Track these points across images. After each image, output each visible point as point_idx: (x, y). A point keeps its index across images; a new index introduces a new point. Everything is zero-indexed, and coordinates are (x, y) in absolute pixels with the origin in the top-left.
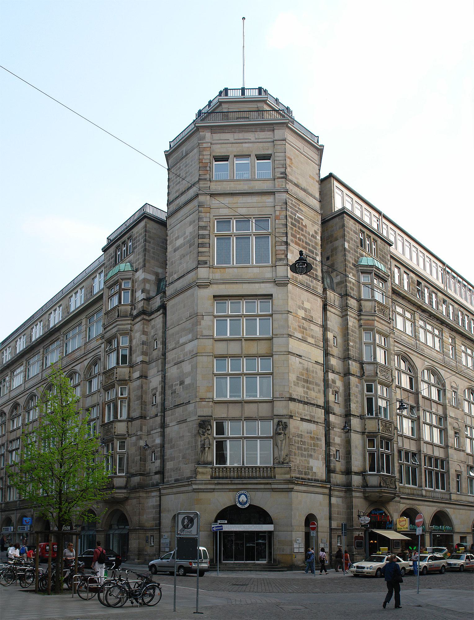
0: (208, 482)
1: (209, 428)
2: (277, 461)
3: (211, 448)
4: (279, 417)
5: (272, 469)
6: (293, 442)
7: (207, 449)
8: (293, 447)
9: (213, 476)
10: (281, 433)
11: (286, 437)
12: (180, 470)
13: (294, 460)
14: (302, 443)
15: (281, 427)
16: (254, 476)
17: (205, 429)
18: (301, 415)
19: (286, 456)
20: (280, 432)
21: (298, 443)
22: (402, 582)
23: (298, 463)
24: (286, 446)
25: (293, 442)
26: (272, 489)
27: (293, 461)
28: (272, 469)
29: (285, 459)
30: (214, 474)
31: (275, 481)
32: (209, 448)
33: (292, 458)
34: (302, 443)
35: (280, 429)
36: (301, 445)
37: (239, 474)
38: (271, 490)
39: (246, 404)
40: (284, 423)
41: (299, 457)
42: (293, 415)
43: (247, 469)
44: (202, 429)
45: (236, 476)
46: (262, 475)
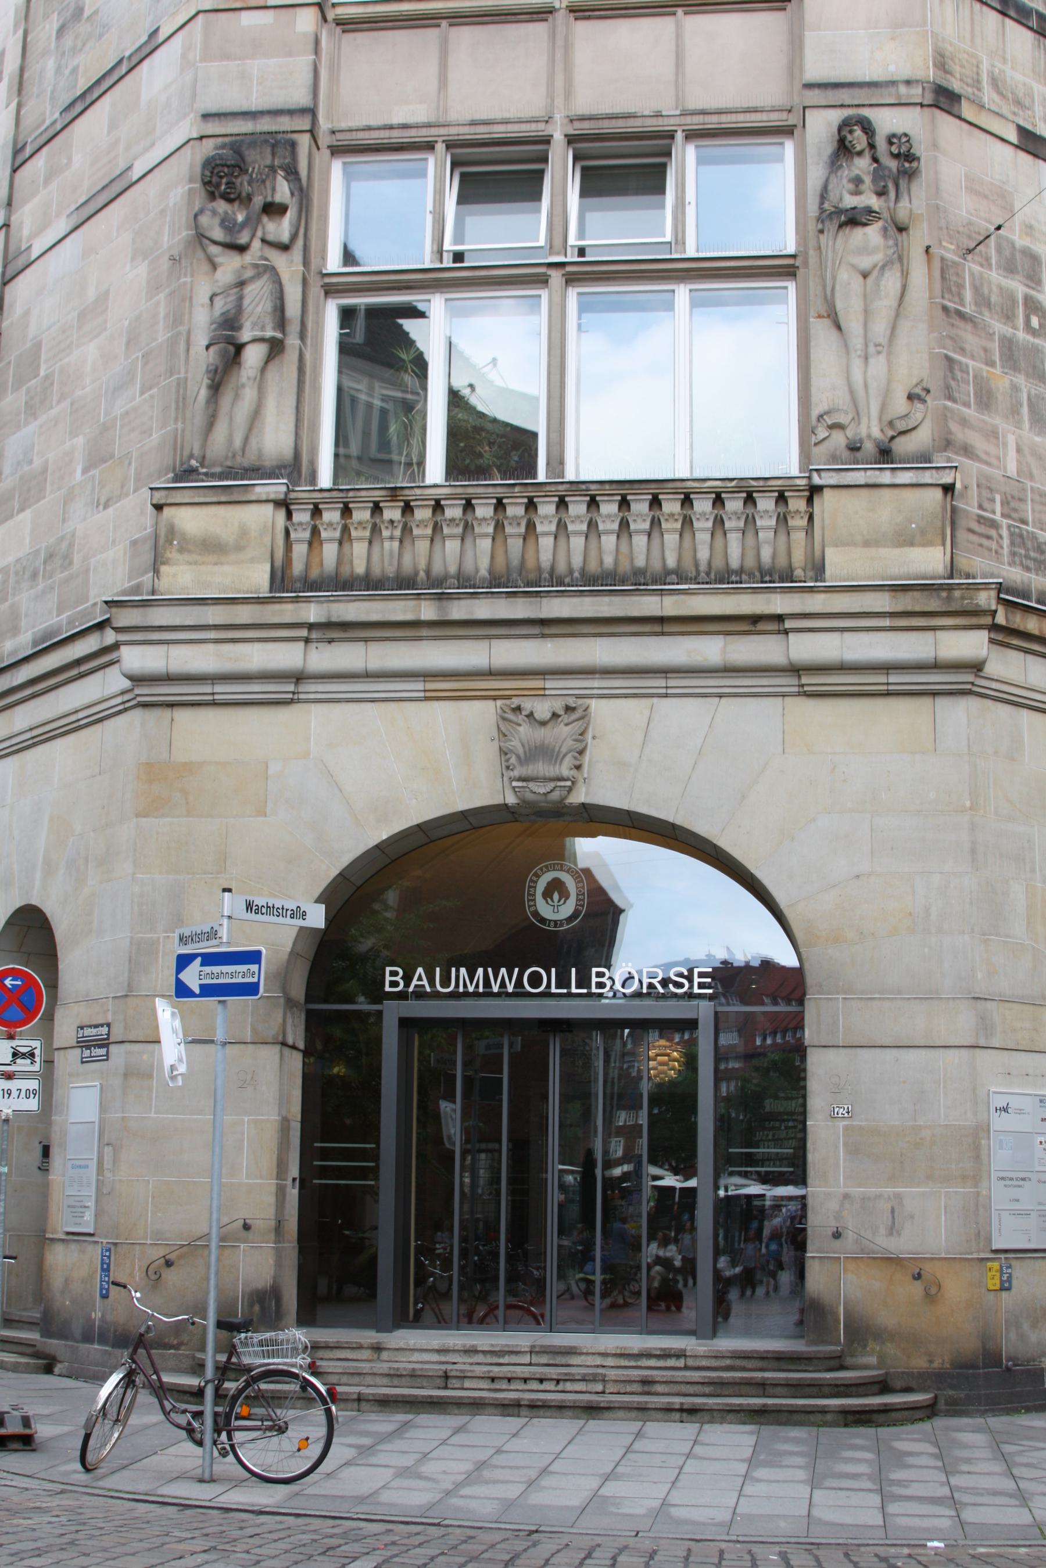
0: (244, 614)
1: (283, 191)
2: (839, 440)
3: (291, 356)
4: (844, 96)
5: (797, 504)
6: (968, 295)
7: (253, 355)
8: (970, 339)
9: (298, 567)
10: (869, 211)
11: (900, 259)
12: (67, 560)
13: (979, 443)
14: (1035, 322)
15: (862, 165)
16: (640, 562)
17: (246, 200)
18: (1018, 103)
19: (911, 397)
20: (850, 201)
21: (1009, 317)
22: (865, 1346)
23: (1012, 469)
24: (904, 325)
25: (968, 295)
26: (796, 670)
27: (967, 451)
28: (797, 504)
29: (901, 426)
30: (300, 551)
31: (816, 603)
32: (276, 348)
33: (964, 422)
34: (1035, 322)
35: (858, 181)
36: (1034, 332)
37: (515, 545)
38: (788, 682)
39: (583, 29)
40: (890, 140)
41: (1018, 425)
42: (956, 86)
43: (578, 508)
44: (221, 206)
45: (484, 572)
46: (703, 554)
